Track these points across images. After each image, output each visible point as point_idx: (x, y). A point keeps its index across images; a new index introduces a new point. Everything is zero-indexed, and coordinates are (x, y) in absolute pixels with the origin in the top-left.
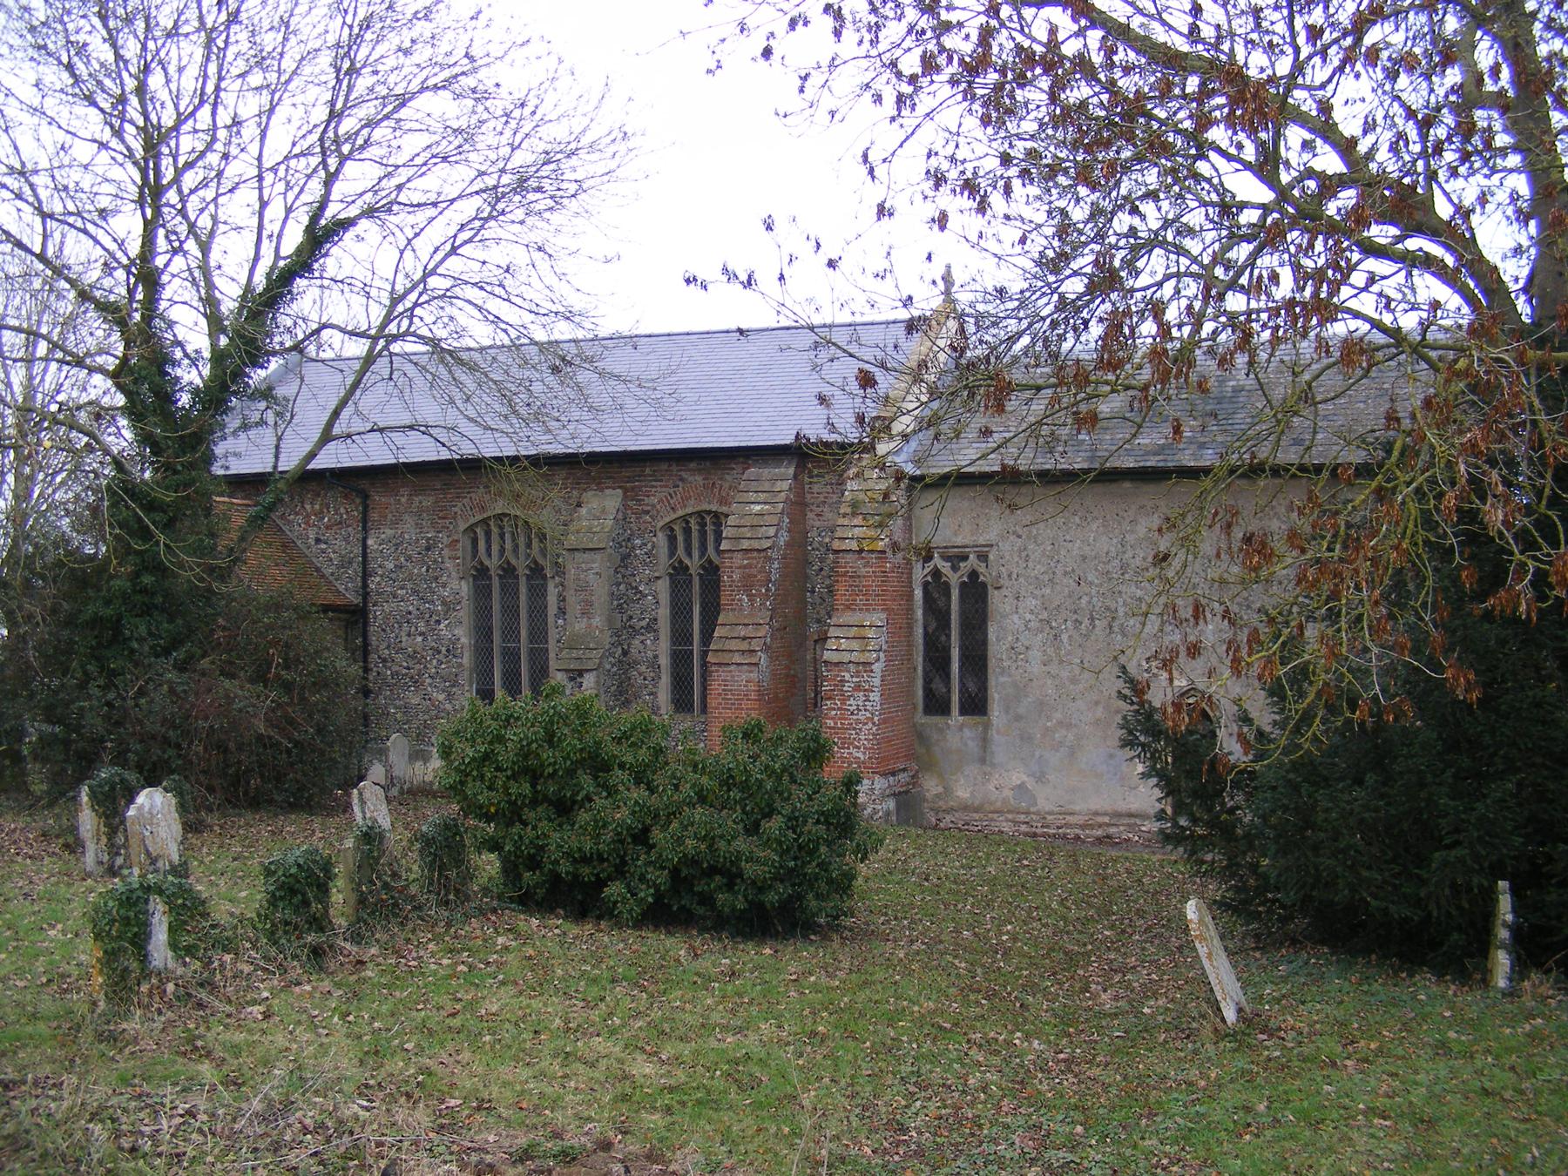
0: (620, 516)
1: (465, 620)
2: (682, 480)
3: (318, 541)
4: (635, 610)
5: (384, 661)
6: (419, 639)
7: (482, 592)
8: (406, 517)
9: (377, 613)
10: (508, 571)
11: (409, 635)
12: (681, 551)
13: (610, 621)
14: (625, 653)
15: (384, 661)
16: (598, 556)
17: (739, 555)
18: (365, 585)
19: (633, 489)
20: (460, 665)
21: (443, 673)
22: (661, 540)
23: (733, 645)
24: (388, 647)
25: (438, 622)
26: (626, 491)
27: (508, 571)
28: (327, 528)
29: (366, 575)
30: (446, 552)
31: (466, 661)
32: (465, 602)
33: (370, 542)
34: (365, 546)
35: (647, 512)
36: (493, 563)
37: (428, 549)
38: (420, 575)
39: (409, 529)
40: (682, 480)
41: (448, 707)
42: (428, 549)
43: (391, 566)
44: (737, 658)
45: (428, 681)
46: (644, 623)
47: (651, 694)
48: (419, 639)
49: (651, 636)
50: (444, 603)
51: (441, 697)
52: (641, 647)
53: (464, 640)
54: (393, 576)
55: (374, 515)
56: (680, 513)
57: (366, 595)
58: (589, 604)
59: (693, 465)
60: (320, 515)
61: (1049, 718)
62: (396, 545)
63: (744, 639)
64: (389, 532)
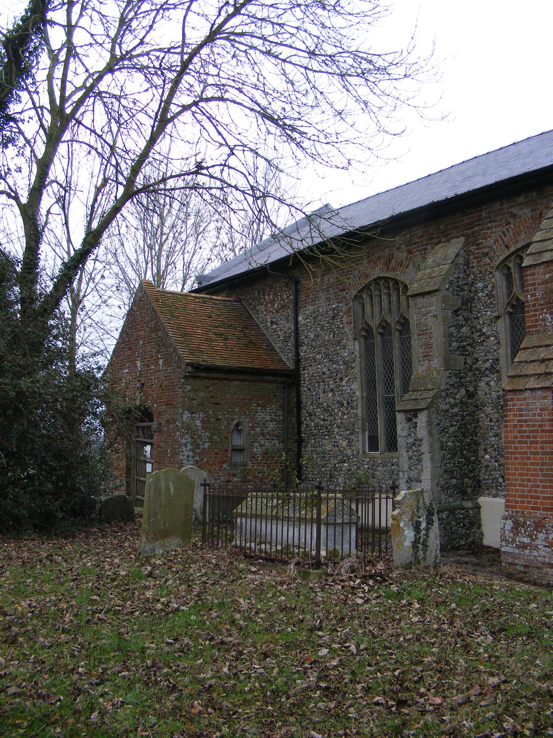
0: (461, 260)
1: (358, 376)
2: (514, 216)
3: (272, 322)
4: (479, 352)
5: (310, 415)
6: (330, 395)
7: (369, 350)
8: (320, 294)
9: (305, 374)
10: (385, 326)
11: (324, 392)
12: (516, 289)
13: (447, 363)
14: (471, 395)
15: (310, 415)
16: (434, 299)
17: (541, 270)
18: (297, 354)
19: (473, 233)
20: (356, 415)
21: (346, 422)
22: (499, 278)
23: (530, 369)
24: (312, 404)
25: (341, 379)
26: (467, 237)
27: (385, 326)
28: (277, 312)
29: (298, 345)
30: (345, 319)
31: (359, 412)
32: (358, 360)
33: (300, 318)
34: (296, 323)
35: (487, 254)
36: (374, 323)
37: (333, 318)
38: (329, 341)
39: (322, 305)
40: (514, 216)
41: (349, 452)
42: (333, 318)
43: (312, 336)
44: (532, 383)
45: (336, 430)
46: (488, 365)
47: (496, 435)
48: (330, 395)
49: (494, 376)
50: (345, 363)
51: (344, 444)
52: (487, 389)
53: (358, 393)
54: (314, 344)
55: (302, 297)
56: (513, 249)
57: (298, 361)
58: (429, 346)
59: (521, 199)
60: (272, 302)
61: (50, 444)
62: (315, 318)
63: (543, 361)
64: (311, 308)
